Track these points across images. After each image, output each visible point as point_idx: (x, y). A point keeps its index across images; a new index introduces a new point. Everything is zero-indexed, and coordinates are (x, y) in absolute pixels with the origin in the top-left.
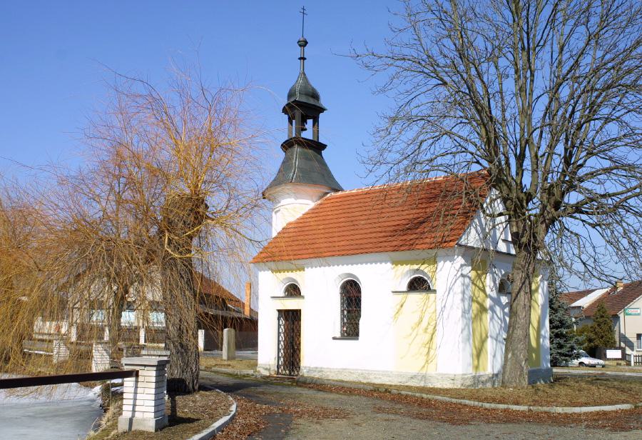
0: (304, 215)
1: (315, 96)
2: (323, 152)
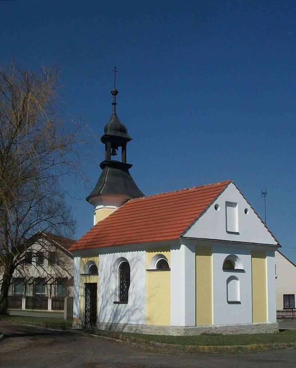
0: (110, 215)
1: (123, 130)
2: (130, 170)
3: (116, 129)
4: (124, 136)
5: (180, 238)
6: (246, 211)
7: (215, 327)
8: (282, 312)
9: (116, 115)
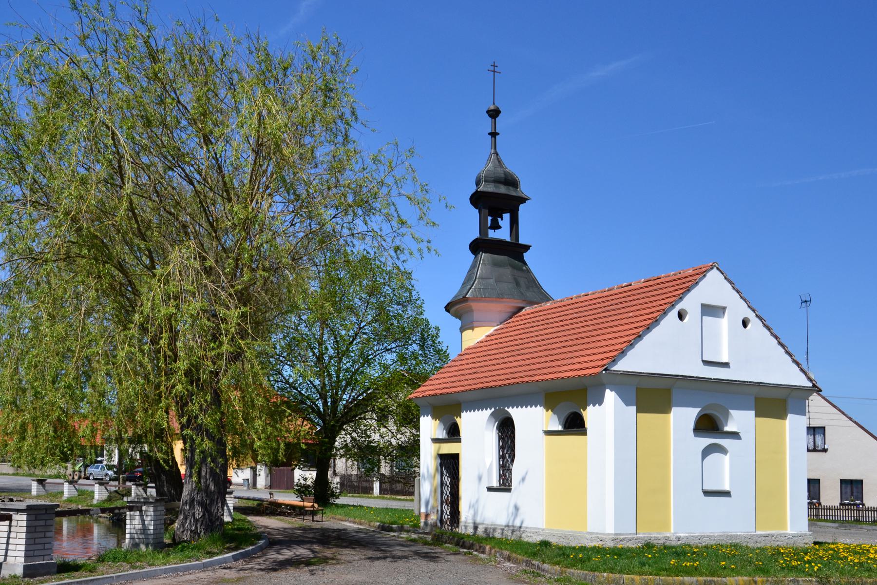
1: (511, 181)
2: (527, 256)
3: (497, 181)
4: (514, 194)
5: (604, 372)
6: (745, 323)
7: (677, 537)
8: (837, 509)
9: (497, 155)
